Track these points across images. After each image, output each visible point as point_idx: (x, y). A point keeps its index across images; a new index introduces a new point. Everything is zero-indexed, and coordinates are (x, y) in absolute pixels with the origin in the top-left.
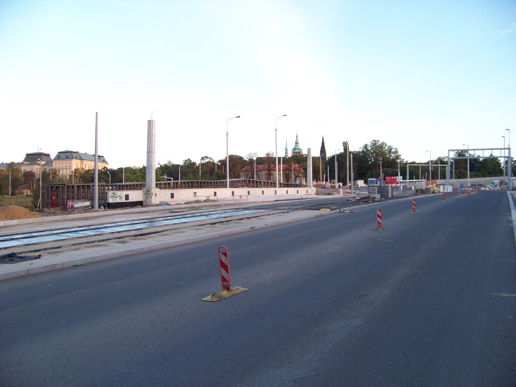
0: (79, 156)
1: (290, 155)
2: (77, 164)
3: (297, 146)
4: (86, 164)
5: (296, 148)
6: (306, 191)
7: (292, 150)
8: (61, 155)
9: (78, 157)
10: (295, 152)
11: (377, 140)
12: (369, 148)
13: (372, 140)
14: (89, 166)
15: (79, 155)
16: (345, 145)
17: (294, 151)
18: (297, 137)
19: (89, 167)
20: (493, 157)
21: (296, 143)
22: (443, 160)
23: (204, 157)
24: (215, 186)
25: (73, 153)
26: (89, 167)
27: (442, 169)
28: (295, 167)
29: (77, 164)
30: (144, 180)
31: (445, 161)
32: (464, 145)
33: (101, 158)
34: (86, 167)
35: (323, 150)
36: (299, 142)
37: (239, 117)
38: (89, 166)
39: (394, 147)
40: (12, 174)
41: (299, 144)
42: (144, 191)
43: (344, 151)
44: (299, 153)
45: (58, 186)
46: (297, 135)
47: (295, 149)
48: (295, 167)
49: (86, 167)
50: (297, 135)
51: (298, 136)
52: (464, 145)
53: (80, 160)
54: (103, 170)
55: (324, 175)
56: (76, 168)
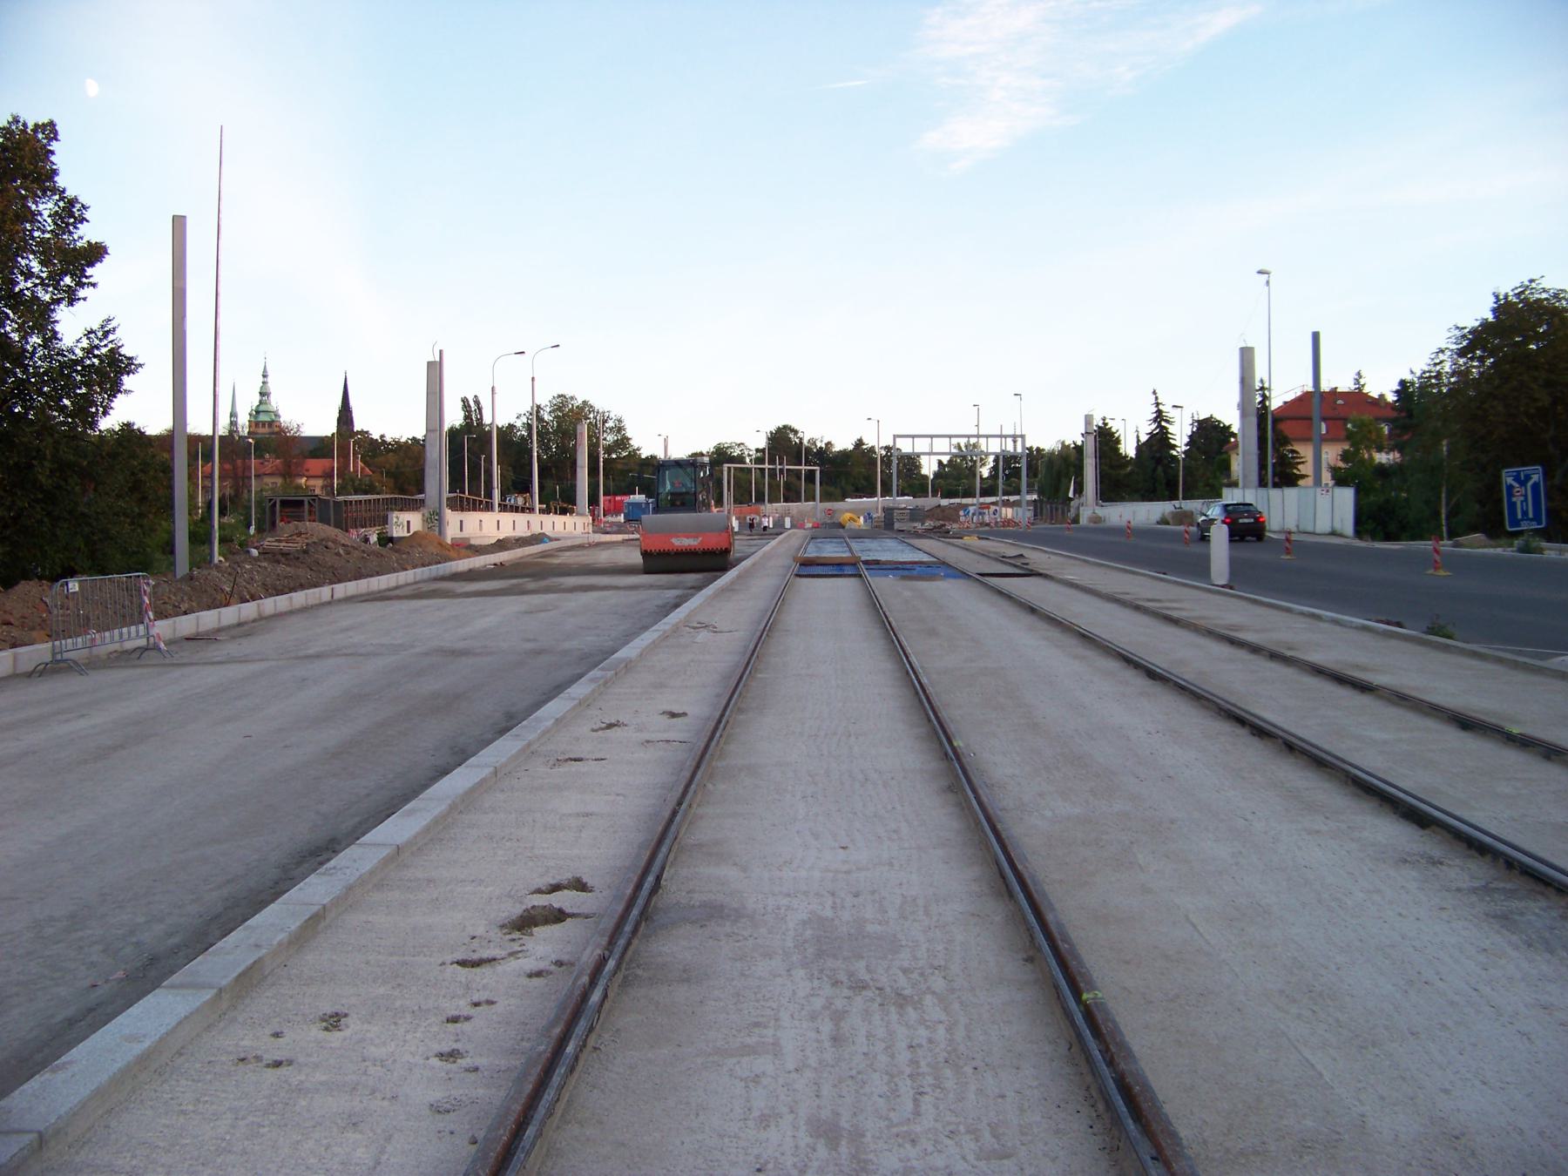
3: (266, 403)
5: (262, 408)
7: (250, 415)
11: (569, 394)
12: (547, 417)
13: (556, 396)
17: (256, 417)
18: (264, 376)
20: (171, 465)
21: (260, 393)
22: (729, 451)
24: (525, 488)
27: (739, 474)
30: (169, 452)
31: (735, 454)
32: (869, 419)
36: (271, 391)
39: (612, 415)
40: (205, 548)
41: (272, 398)
42: (423, 515)
44: (271, 423)
46: (265, 370)
47: (258, 412)
50: (265, 370)
51: (269, 372)
52: (869, 419)
55: (352, 469)
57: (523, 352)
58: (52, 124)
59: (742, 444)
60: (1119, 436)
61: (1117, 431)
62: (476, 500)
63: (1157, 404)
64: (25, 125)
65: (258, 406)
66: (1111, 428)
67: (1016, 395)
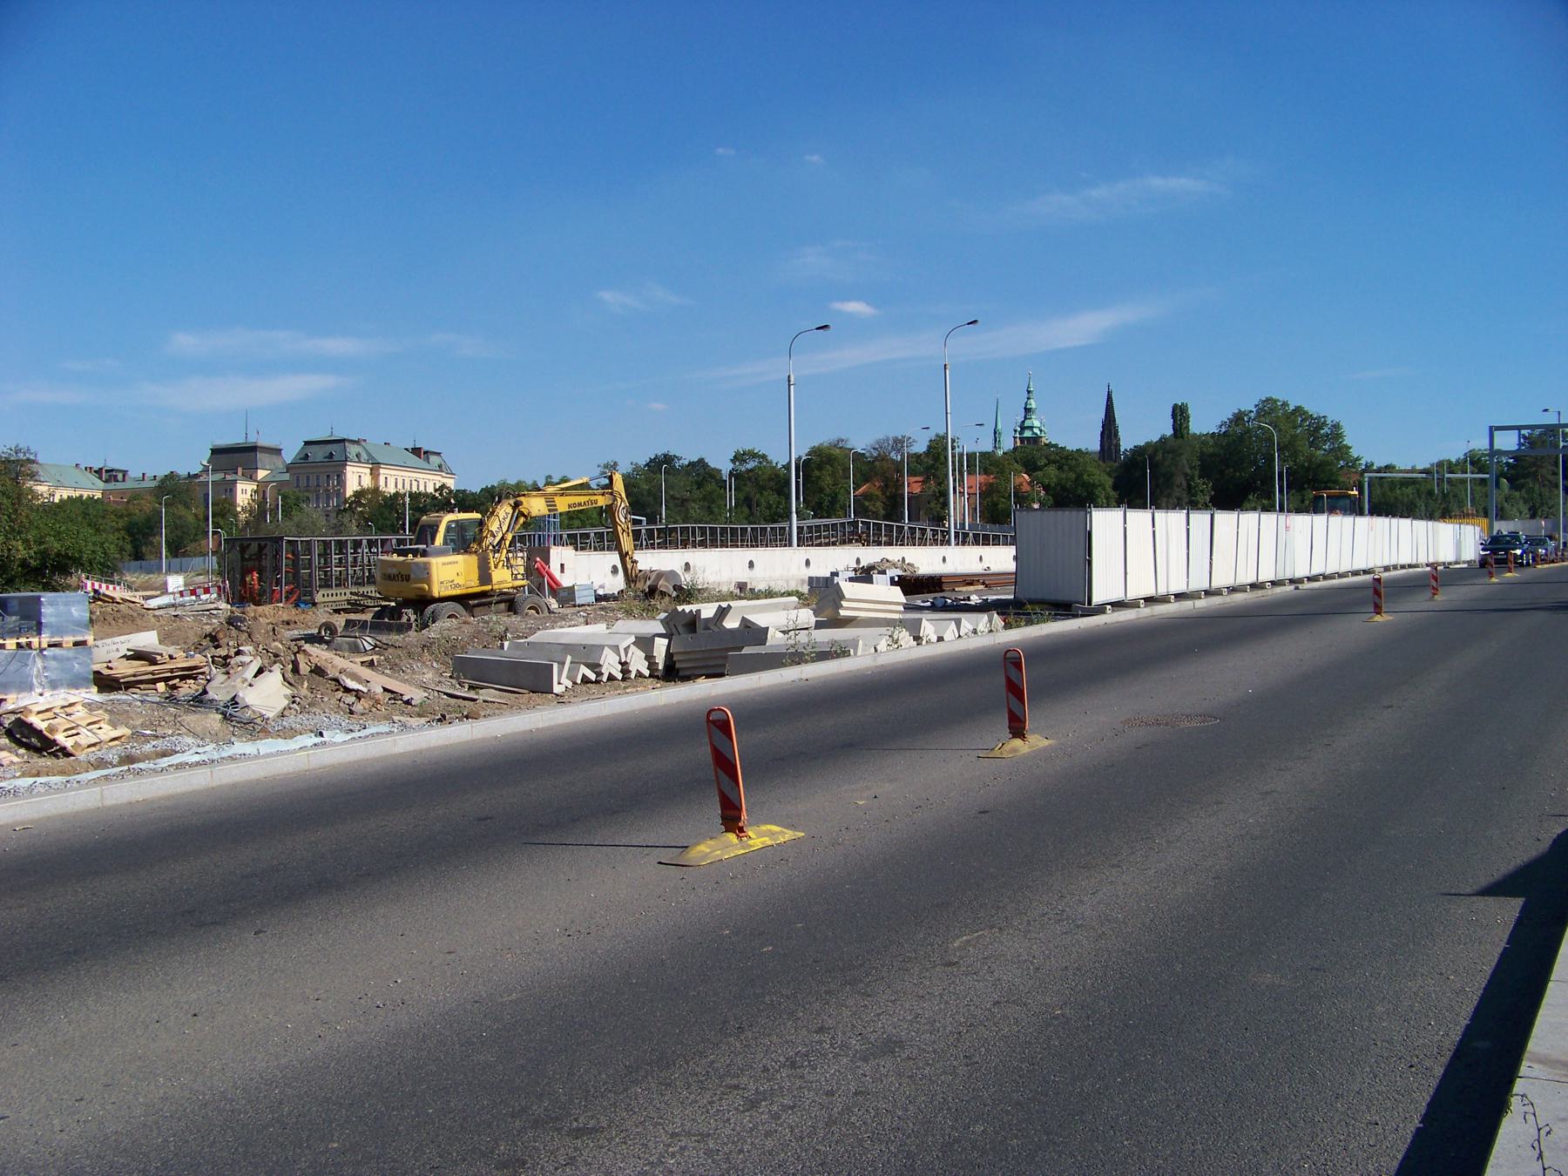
0: (368, 453)
1: (1008, 444)
2: (360, 476)
4: (362, 475)
6: (559, 566)
8: (311, 450)
9: (364, 456)
10: (1024, 436)
14: (396, 483)
15: (367, 451)
16: (1180, 414)
19: (396, 486)
23: (744, 454)
24: (757, 541)
25: (347, 444)
26: (396, 486)
28: (1021, 484)
29: (360, 476)
32: (1546, 410)
33: (432, 458)
34: (386, 485)
35: (1109, 428)
37: (975, 322)
38: (396, 483)
43: (1172, 432)
45: (245, 543)
48: (1021, 484)
49: (386, 485)
52: (1546, 410)
53: (371, 466)
54: (437, 495)
56: (359, 488)
65: (1024, 421)
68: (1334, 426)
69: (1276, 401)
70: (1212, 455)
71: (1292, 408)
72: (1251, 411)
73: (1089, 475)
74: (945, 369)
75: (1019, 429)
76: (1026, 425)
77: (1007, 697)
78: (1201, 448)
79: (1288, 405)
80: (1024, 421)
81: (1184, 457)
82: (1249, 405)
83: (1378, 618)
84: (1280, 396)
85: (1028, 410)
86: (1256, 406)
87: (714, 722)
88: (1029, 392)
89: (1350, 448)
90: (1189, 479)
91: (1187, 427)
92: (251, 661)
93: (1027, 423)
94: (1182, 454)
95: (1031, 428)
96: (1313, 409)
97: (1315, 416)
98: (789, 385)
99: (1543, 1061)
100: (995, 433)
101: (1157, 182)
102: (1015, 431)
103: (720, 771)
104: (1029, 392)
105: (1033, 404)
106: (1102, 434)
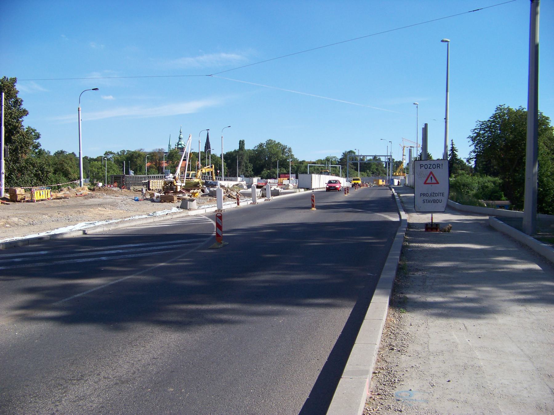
16: (242, 143)
57: (230, 126)
58: (15, 79)
59: (335, 157)
60: (431, 156)
61: (431, 154)
62: (136, 177)
63: (452, 145)
64: (7, 79)
65: (179, 142)
66: (429, 153)
67: (390, 142)
68: (289, 149)
69: (272, 140)
70: (252, 156)
71: (277, 142)
72: (264, 143)
73: (219, 162)
74: (79, 110)
75: (177, 145)
76: (179, 143)
77: (216, 219)
78: (249, 154)
79: (276, 142)
80: (179, 142)
81: (245, 157)
82: (264, 142)
83: (345, 195)
84: (273, 139)
85: (180, 138)
86: (266, 142)
87: (218, 216)
88: (180, 132)
89: (294, 155)
90: (246, 163)
91: (244, 148)
92: (234, 198)
93: (180, 143)
94: (244, 156)
95: (181, 144)
96: (283, 143)
97: (283, 145)
98: (199, 143)
99: (432, 216)
100: (169, 146)
101: (224, 55)
102: (176, 145)
103: (221, 225)
104: (180, 132)
105: (182, 136)
106: (205, 147)
